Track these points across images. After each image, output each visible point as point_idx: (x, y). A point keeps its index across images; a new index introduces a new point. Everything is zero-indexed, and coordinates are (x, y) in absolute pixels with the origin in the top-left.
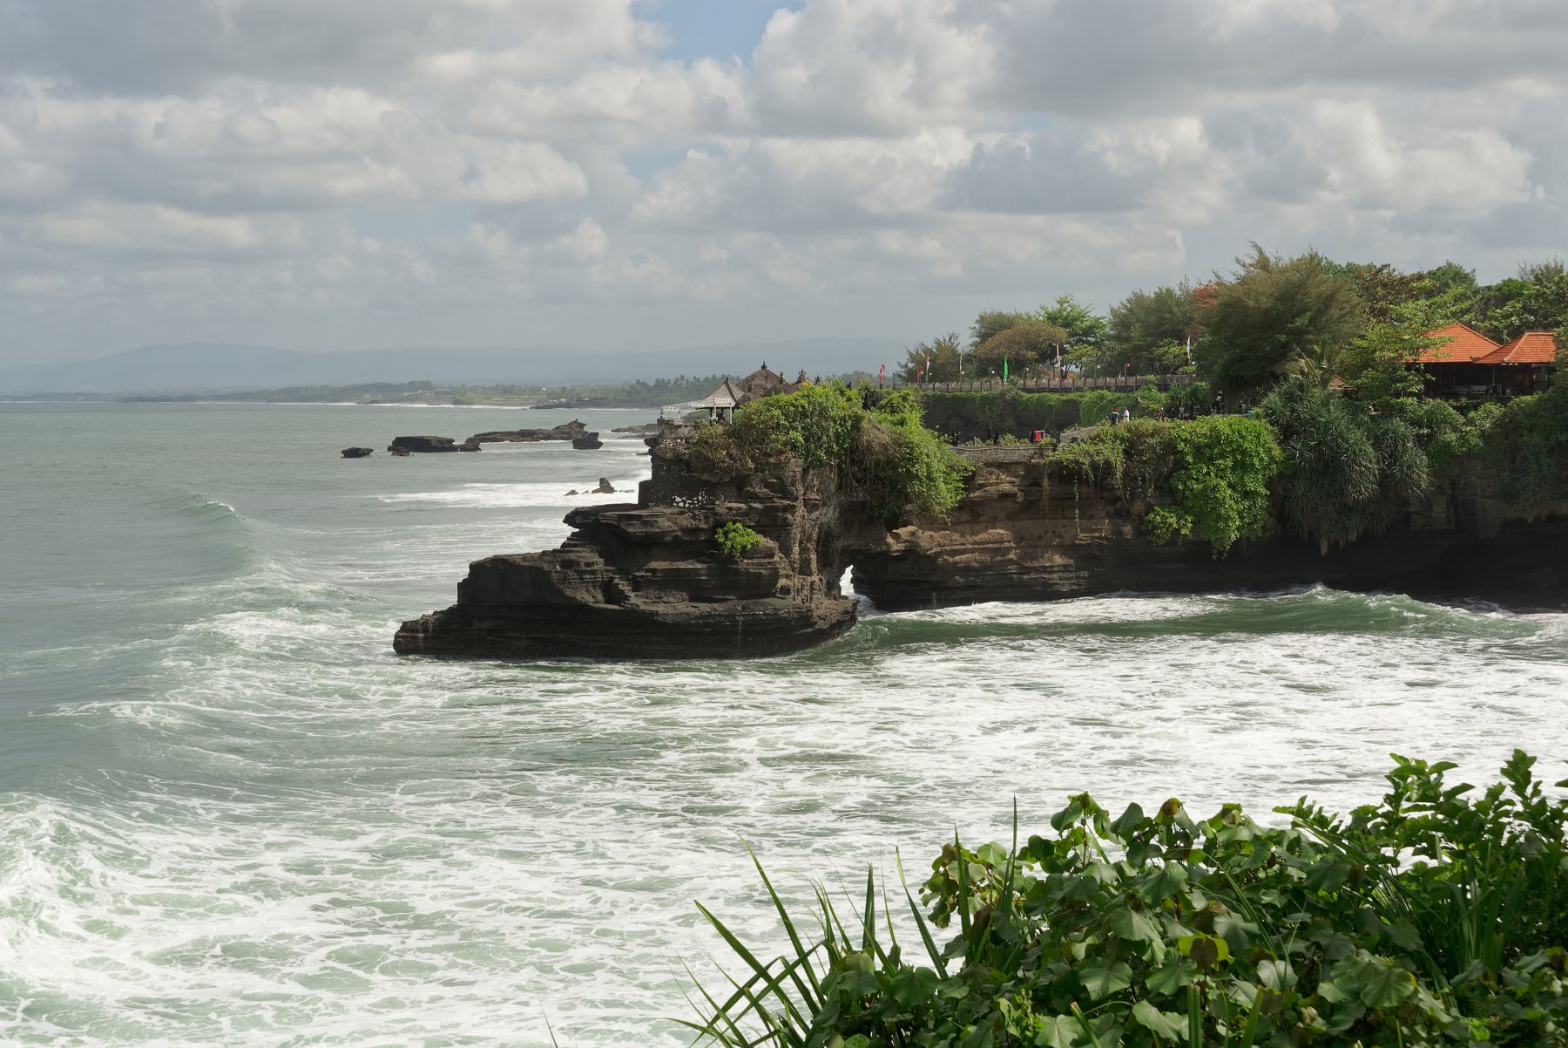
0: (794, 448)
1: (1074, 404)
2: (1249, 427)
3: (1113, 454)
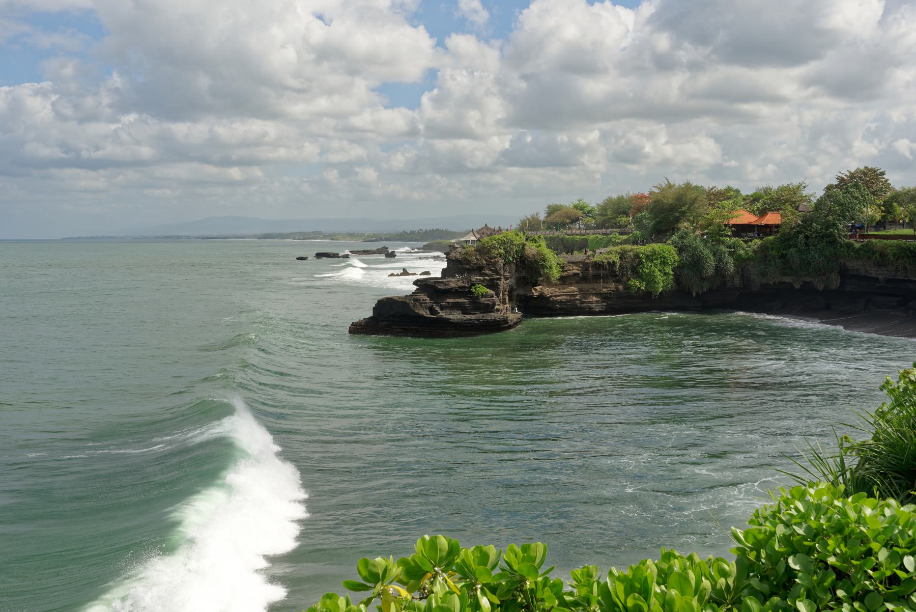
0: (501, 256)
1: (586, 240)
2: (667, 249)
3: (615, 258)
